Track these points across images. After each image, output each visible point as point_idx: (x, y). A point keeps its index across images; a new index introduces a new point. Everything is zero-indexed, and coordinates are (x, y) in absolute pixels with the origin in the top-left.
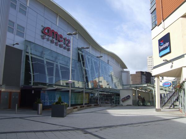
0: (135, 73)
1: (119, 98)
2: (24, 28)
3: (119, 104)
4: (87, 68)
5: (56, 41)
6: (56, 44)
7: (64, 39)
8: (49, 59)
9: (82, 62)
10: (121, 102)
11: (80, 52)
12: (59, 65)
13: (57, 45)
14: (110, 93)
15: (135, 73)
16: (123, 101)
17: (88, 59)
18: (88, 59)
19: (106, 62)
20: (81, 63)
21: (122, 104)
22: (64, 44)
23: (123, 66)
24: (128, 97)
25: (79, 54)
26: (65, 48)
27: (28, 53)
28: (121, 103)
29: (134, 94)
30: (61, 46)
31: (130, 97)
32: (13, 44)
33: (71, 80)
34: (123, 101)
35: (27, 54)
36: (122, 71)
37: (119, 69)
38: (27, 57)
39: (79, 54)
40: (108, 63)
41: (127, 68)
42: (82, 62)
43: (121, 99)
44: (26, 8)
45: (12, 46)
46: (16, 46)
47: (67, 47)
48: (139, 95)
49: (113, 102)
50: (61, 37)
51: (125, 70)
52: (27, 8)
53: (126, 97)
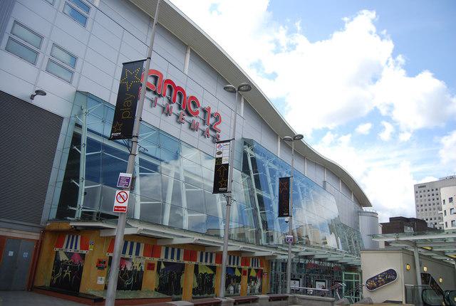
0: (388, 221)
1: (357, 277)
2: (42, 38)
3: (357, 294)
4: (268, 192)
5: (179, 112)
6: (179, 120)
7: (205, 111)
8: (192, 171)
9: (252, 175)
10: (365, 289)
11: (248, 150)
12: (85, 136)
13: (180, 123)
14: (329, 264)
15: (388, 221)
16: (371, 288)
17: (302, 189)
18: (302, 189)
19: (321, 185)
20: (250, 178)
21: (369, 299)
22: (204, 123)
23: (362, 200)
24: (390, 276)
25: (245, 155)
26: (204, 134)
27: (80, 127)
28: (365, 293)
29: (408, 267)
30: (193, 127)
31: (395, 275)
32: (30, 94)
33: (190, 219)
34: (371, 288)
35: (78, 131)
36: (358, 212)
37: (350, 203)
38: (76, 139)
39: (245, 155)
40: (324, 188)
41: (370, 205)
42: (252, 175)
43: (364, 283)
44: (89, 8)
45: (29, 100)
46: (39, 101)
47: (211, 133)
48: (425, 269)
49: (340, 291)
50: (194, 102)
51: (365, 209)
52: (93, 10)
53: (384, 275)
